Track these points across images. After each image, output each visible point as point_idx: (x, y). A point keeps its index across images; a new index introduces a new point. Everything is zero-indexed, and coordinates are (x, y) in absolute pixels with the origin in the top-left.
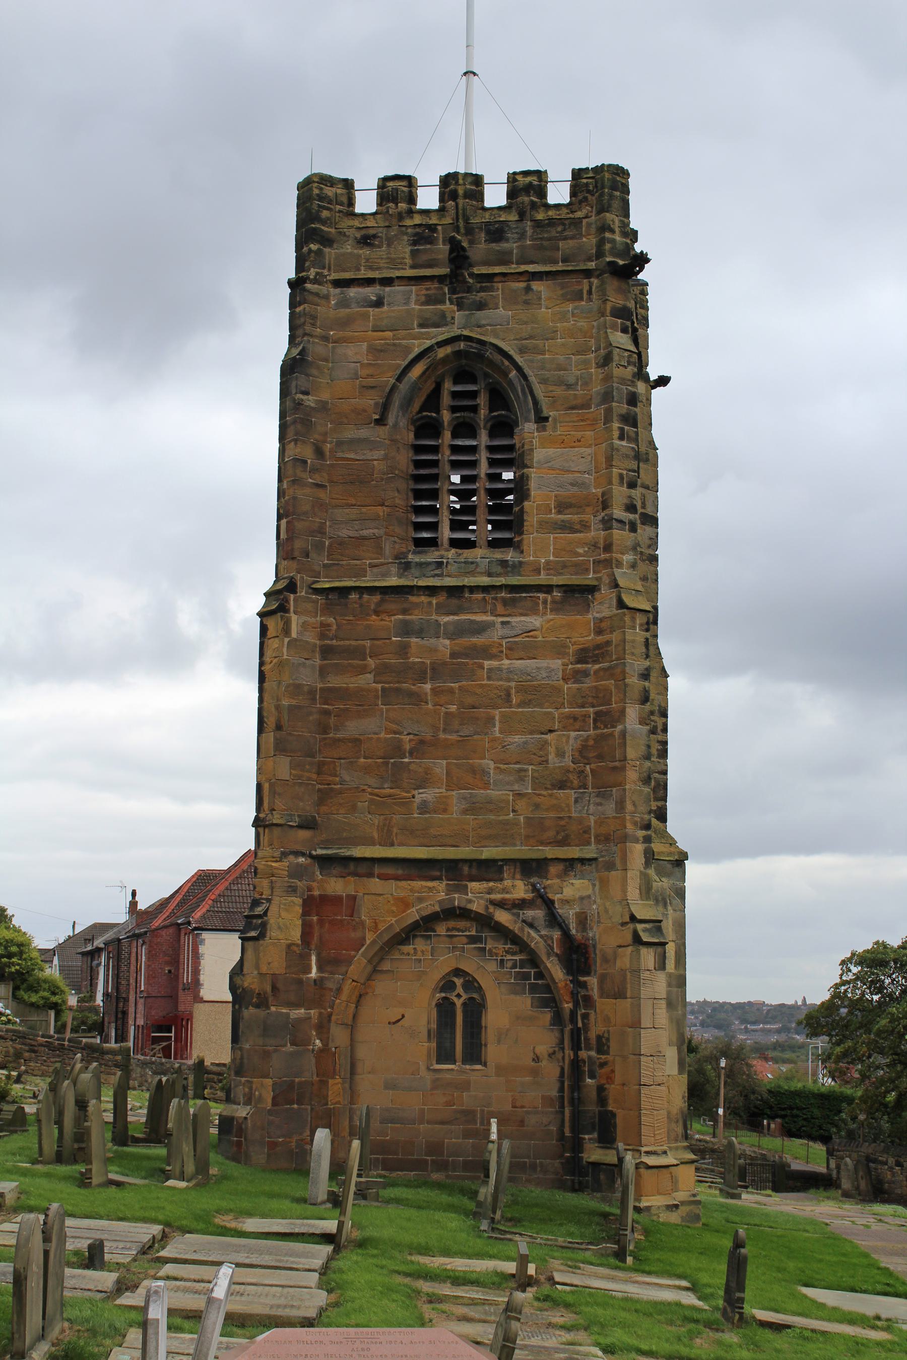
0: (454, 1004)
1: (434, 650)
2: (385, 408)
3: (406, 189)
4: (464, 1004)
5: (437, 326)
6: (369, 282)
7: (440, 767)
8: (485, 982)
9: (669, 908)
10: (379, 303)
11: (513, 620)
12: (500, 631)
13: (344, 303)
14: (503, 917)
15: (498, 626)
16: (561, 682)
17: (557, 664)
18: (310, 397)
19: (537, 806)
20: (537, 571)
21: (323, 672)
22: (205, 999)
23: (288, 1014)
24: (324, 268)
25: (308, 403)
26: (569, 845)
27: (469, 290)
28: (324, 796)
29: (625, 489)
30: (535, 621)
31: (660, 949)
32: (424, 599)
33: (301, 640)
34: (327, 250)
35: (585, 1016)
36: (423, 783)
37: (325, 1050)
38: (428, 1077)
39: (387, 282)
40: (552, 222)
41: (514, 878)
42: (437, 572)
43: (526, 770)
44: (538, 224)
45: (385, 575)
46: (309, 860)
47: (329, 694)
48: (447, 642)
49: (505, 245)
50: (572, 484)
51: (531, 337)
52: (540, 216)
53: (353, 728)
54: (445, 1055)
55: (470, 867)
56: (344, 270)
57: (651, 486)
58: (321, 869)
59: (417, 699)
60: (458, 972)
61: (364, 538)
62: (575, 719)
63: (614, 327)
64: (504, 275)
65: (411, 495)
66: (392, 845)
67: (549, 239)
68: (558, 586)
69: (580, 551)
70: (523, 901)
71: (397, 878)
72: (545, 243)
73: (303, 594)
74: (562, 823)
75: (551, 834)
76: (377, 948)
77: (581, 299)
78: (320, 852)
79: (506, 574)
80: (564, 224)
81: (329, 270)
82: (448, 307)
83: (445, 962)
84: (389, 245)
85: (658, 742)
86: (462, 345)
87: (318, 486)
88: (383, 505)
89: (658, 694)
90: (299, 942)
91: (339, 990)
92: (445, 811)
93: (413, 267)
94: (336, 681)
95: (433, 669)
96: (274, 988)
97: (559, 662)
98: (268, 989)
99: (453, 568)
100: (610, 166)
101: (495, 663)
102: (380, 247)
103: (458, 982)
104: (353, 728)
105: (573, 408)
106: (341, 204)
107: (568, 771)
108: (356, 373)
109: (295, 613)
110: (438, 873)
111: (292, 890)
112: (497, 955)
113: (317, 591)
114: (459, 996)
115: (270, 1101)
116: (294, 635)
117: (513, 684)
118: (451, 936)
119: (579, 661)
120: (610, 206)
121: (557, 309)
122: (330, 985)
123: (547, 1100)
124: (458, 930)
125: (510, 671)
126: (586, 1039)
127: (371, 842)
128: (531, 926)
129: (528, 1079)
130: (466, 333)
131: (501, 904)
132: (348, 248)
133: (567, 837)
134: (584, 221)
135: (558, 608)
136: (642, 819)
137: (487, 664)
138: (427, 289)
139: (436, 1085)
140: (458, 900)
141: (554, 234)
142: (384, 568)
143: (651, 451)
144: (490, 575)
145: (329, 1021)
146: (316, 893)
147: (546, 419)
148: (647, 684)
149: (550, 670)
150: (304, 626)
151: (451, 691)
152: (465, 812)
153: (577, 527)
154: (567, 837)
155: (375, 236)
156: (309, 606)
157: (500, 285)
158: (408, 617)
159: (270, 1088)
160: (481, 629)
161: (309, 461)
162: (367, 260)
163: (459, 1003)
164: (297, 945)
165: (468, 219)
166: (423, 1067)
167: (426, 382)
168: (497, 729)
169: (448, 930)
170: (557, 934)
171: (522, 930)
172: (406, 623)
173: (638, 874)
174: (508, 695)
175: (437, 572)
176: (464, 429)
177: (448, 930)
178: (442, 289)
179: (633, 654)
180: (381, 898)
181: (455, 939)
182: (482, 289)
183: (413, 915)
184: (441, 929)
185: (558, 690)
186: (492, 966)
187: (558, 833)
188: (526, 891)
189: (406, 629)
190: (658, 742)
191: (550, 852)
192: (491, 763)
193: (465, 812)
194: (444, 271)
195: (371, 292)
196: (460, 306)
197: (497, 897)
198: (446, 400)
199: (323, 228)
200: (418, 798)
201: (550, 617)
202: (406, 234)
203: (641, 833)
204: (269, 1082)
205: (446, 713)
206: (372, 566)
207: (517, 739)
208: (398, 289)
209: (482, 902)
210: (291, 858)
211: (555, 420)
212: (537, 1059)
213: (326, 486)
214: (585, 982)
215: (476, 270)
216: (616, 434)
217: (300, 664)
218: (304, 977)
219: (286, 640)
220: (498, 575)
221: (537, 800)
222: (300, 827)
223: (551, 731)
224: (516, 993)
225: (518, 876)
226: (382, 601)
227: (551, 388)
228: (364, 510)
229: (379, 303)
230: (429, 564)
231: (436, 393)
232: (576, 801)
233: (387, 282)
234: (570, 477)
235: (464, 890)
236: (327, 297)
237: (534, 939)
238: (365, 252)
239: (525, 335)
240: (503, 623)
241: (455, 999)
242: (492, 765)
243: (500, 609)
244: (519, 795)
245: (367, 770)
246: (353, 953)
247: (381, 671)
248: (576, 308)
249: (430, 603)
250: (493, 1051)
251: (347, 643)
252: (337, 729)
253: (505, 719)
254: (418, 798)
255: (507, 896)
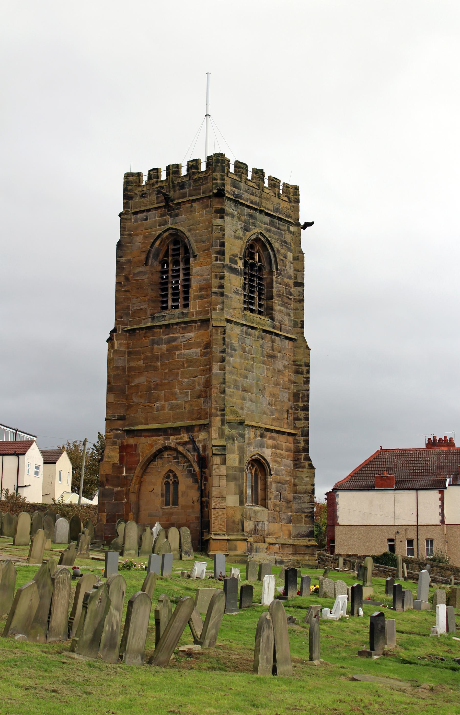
0: (169, 483)
1: (161, 349)
2: (147, 259)
3: (156, 174)
4: (173, 483)
5: (163, 225)
6: (143, 211)
7: (162, 393)
8: (178, 474)
9: (236, 441)
10: (146, 219)
11: (185, 335)
12: (181, 340)
13: (136, 221)
14: (180, 448)
15: (181, 338)
16: (200, 357)
17: (198, 350)
18: (123, 258)
19: (191, 405)
20: (193, 315)
21: (128, 361)
22: (340, 524)
23: (113, 489)
24: (129, 208)
25: (122, 261)
26: (201, 419)
27: (173, 210)
28: (129, 407)
29: (218, 280)
30: (192, 335)
31: (223, 457)
32: (158, 330)
33: (119, 350)
34: (130, 201)
35: (205, 485)
36: (157, 400)
37: (128, 502)
38: (161, 511)
39: (148, 210)
40: (199, 179)
41: (184, 433)
42: (163, 319)
43: (188, 392)
44: (195, 181)
45: (147, 323)
46: (122, 432)
47: (131, 369)
48: (165, 346)
49: (185, 190)
50: (204, 280)
51: (192, 225)
52: (195, 177)
53: (137, 381)
54: (167, 504)
55: (171, 430)
56: (136, 208)
57: (300, 270)
58: (127, 434)
59: (156, 368)
60: (171, 471)
61: (141, 309)
62: (204, 371)
63: (216, 217)
64: (184, 202)
65: (160, 290)
66: (148, 424)
67: (198, 186)
68: (199, 320)
69: (206, 306)
70: (186, 442)
71: (149, 436)
72: (197, 187)
73: (120, 332)
74: (199, 411)
75: (195, 416)
76: (143, 463)
77: (208, 207)
78: (126, 428)
79: (183, 317)
80: (203, 179)
81: (131, 208)
82: (167, 217)
83: (166, 468)
84: (150, 196)
85: (304, 377)
86: (171, 231)
87: (126, 291)
88: (147, 296)
89: (304, 357)
90: (118, 462)
91: (132, 480)
92: (164, 410)
93: (157, 203)
94: (132, 364)
95: (161, 356)
96: (107, 480)
97: (199, 349)
98: (104, 479)
99: (167, 317)
100: (173, 165)
101: (179, 352)
102: (147, 197)
103: (171, 474)
104: (137, 381)
105: (205, 251)
106: (136, 183)
107: (201, 391)
108: (139, 247)
109: (116, 340)
110: (161, 434)
111: (115, 443)
112: (182, 463)
113: (126, 331)
114: (171, 480)
115: (105, 521)
116: (116, 348)
117: (185, 359)
118: (168, 457)
119: (205, 348)
120: (215, 170)
121: (200, 213)
122: (129, 478)
123: (197, 518)
124: (171, 455)
125: (184, 355)
126: (205, 493)
127: (142, 424)
128: (189, 451)
129: (191, 510)
130: (172, 226)
131: (179, 444)
132: (137, 199)
133: (200, 417)
134: (209, 177)
135: (199, 328)
136: (220, 407)
137: (177, 352)
138: (161, 211)
139: (164, 514)
140: (167, 443)
141: (200, 183)
142: (147, 320)
143: (300, 256)
144: (179, 318)
145: (129, 491)
146: (125, 444)
147: (196, 256)
148: (224, 355)
149: (196, 353)
150: (120, 344)
151: (166, 364)
152: (170, 410)
153: (205, 296)
154: (200, 417)
155: (145, 193)
156: (123, 337)
157: (183, 206)
158: (153, 338)
159: (105, 516)
160: (175, 339)
161: (122, 283)
162: (143, 203)
163: (171, 482)
164: (117, 464)
165: (173, 182)
166: (159, 507)
167: (163, 246)
168: (180, 377)
169: (168, 455)
170: (196, 454)
171: (186, 453)
172: (153, 340)
173: (218, 428)
174: (183, 364)
175: (163, 319)
176: (176, 263)
177: (168, 455)
178: (165, 210)
179: (216, 344)
180: (144, 444)
181: (170, 458)
182: (178, 209)
183: (154, 450)
184: (166, 454)
185: (198, 360)
186: (180, 468)
187: (198, 415)
188: (188, 438)
189: (153, 342)
190: (304, 377)
191: (194, 422)
192: (178, 390)
193: (170, 410)
194: (163, 204)
195: (143, 215)
196: (171, 216)
197: (178, 441)
198: (170, 252)
199: (128, 193)
200: (156, 406)
201: (197, 332)
202: (155, 191)
203: (219, 413)
204: (105, 514)
205: (165, 373)
206: (144, 319)
207: (186, 380)
208: (153, 212)
209: (174, 443)
210: (114, 431)
211: (199, 256)
212: (193, 503)
213: (130, 291)
214: (205, 472)
215: (175, 202)
216: (214, 259)
217: (118, 359)
218: (120, 475)
219: (112, 351)
220: (181, 318)
221: (192, 403)
222: (118, 419)
223: (197, 376)
224: (187, 478)
225: (185, 433)
226: (146, 332)
227: (198, 244)
228: (141, 298)
229: (146, 219)
230: (160, 316)
231: (167, 251)
232: (204, 402)
233: (148, 210)
234: (203, 277)
235: (168, 439)
236: (130, 219)
237: (189, 455)
238: (143, 200)
239: (190, 224)
240: (182, 336)
241: (170, 481)
242: (178, 391)
243: (181, 331)
244: (186, 402)
245: (141, 397)
246: (136, 466)
247: (146, 358)
248: (206, 211)
249: (160, 331)
250: (181, 500)
251: (135, 349)
252: (132, 382)
253: (182, 373)
254: (156, 406)
255: (182, 440)
